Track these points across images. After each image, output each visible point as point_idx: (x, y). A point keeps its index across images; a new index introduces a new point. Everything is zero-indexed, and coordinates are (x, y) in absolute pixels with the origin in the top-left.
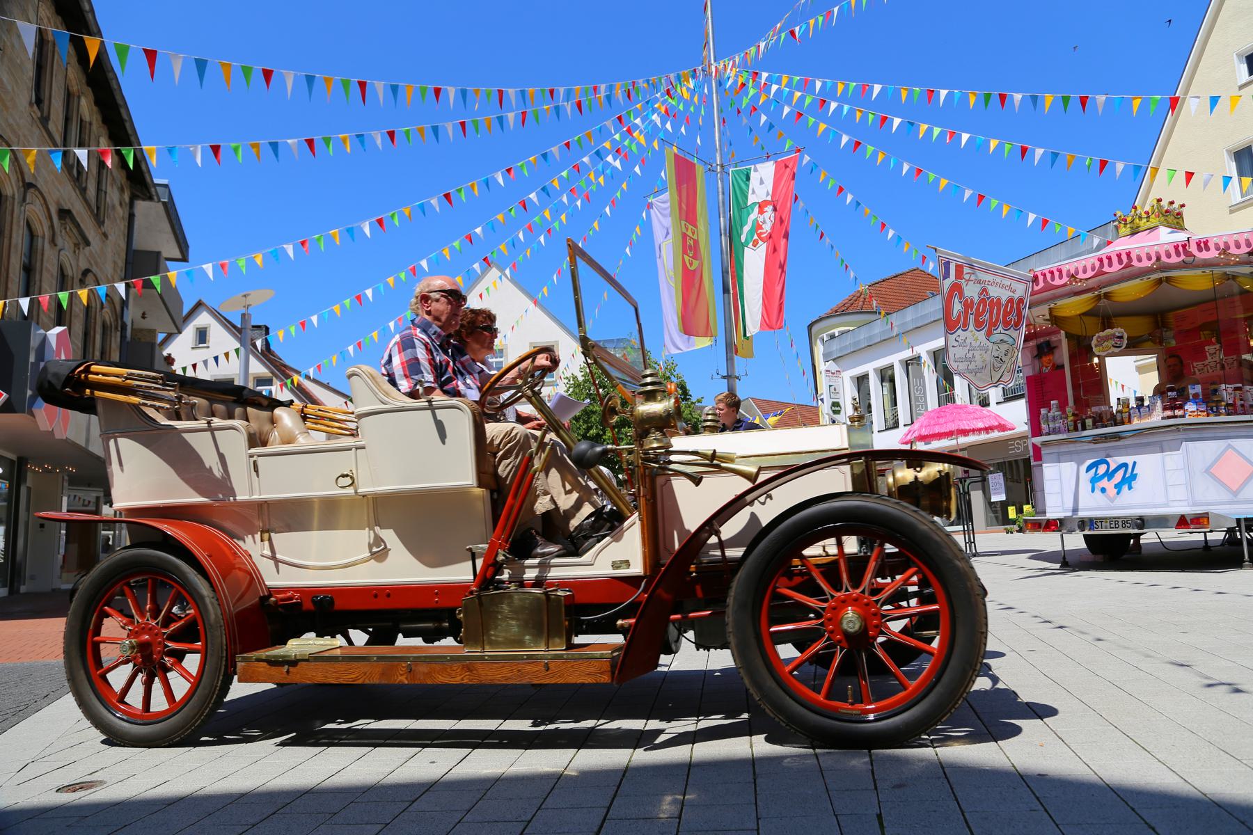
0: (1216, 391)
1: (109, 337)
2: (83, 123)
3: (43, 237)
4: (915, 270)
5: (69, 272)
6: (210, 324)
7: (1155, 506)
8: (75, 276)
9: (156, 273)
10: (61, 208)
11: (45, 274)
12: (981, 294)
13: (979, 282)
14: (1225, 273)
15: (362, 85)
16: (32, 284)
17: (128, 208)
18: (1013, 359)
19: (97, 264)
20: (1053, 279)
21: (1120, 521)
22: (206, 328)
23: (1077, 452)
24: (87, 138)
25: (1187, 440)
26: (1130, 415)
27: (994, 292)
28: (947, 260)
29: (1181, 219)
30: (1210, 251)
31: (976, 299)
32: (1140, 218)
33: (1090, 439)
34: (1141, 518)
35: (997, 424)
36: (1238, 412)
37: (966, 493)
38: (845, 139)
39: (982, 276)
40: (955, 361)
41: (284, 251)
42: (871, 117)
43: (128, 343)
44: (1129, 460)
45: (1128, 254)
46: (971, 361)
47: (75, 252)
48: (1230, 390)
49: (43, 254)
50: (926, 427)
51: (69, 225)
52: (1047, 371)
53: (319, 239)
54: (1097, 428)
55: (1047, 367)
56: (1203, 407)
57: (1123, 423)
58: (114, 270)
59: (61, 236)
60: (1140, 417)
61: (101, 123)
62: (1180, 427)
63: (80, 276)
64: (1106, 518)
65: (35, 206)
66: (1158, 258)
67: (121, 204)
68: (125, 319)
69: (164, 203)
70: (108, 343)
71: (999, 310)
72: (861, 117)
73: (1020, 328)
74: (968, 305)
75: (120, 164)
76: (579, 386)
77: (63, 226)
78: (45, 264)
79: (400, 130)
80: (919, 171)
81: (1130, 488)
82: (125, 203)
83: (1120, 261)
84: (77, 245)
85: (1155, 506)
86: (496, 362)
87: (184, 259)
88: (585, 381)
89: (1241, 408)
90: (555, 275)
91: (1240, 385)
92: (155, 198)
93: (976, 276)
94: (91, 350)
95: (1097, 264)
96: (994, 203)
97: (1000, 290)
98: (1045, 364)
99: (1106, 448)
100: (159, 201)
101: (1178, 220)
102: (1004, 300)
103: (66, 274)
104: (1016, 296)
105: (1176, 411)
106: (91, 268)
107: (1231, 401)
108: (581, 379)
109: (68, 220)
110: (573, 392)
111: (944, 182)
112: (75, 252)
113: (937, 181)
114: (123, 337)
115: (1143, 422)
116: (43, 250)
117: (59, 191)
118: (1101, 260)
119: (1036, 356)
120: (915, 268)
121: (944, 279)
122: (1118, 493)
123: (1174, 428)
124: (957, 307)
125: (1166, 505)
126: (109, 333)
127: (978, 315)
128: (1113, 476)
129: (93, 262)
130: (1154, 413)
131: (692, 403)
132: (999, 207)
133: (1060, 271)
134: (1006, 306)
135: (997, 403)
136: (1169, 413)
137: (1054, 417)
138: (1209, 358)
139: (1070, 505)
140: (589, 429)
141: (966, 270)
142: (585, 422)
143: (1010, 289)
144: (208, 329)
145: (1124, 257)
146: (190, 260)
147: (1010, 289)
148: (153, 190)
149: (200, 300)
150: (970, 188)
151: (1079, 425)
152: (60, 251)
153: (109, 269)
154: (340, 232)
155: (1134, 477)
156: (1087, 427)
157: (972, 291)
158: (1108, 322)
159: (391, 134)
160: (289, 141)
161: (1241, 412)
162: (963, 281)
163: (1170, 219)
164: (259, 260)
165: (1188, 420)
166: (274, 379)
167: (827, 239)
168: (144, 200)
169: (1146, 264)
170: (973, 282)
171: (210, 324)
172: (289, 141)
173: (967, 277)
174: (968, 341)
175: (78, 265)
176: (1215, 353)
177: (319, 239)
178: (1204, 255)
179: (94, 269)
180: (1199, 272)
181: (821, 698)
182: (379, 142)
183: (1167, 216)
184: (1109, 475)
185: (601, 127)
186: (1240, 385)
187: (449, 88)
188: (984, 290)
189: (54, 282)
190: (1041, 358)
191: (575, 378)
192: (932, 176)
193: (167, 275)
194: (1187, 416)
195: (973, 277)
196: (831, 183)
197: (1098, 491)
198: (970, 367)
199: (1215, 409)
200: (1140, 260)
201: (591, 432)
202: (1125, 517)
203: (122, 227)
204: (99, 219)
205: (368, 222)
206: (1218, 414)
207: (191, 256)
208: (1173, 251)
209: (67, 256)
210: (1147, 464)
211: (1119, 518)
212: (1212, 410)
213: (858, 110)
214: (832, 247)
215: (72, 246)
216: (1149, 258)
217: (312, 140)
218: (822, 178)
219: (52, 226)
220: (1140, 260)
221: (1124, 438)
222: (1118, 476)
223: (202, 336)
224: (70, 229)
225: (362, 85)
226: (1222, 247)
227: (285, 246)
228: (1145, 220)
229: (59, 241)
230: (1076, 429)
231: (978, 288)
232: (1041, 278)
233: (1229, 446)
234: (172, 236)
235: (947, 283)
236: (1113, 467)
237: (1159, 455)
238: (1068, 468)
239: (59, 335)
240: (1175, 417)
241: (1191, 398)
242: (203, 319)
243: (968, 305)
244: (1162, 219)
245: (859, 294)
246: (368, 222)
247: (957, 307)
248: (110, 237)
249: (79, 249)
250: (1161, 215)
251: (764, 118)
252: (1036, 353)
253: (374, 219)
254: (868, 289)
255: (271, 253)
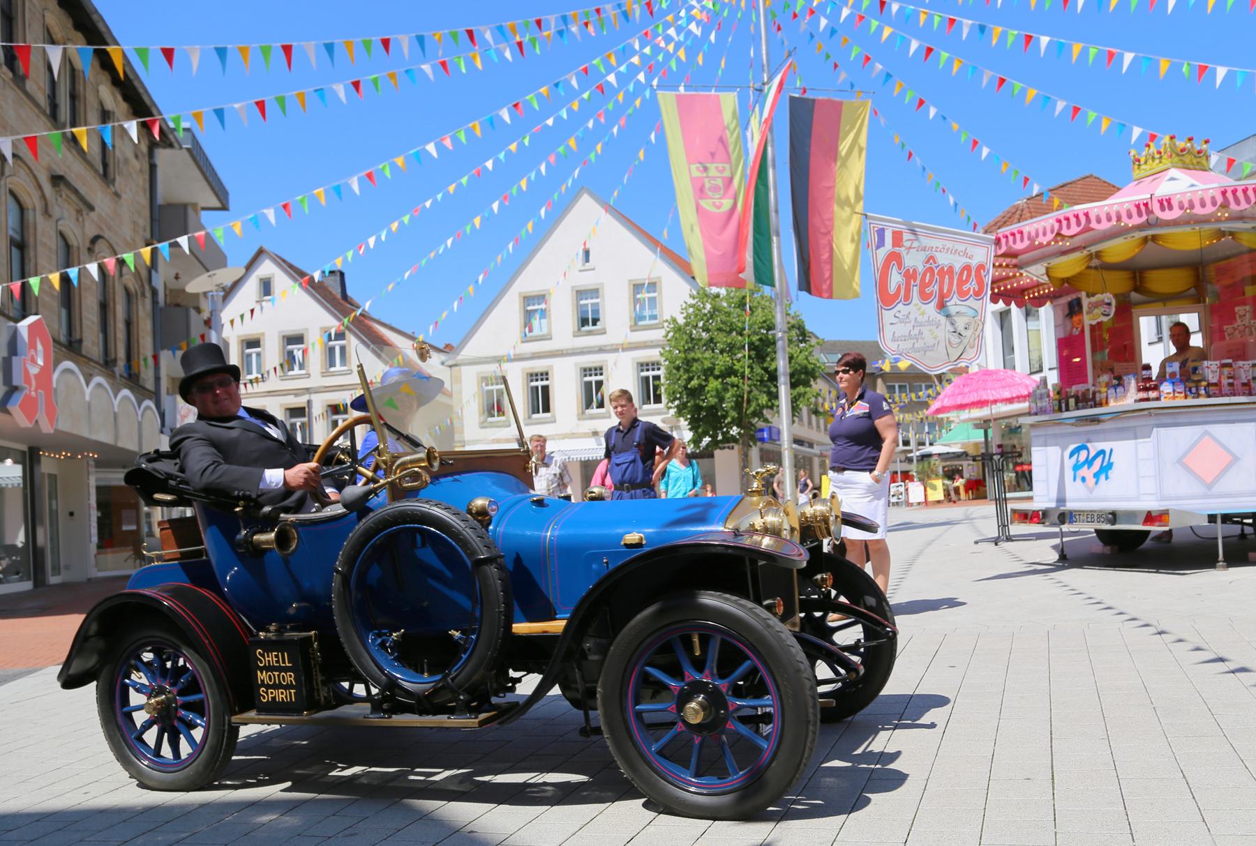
0: (1195, 369)
1: (135, 305)
2: (76, 73)
3: (34, 210)
4: (1087, 177)
5: (73, 241)
6: (273, 274)
7: (1128, 500)
8: (81, 245)
9: (184, 232)
10: (54, 174)
11: (40, 249)
12: (927, 262)
13: (924, 249)
14: (1220, 230)
15: (287, 49)
16: (27, 261)
17: (147, 158)
18: (977, 333)
19: (110, 228)
20: (1015, 242)
21: (1096, 514)
22: (270, 278)
23: (1063, 435)
24: (82, 89)
25: (1159, 426)
26: (1107, 398)
27: (943, 260)
28: (881, 227)
29: (1204, 158)
30: (1173, 212)
31: (921, 269)
32: (1153, 158)
33: (1073, 421)
34: (1114, 514)
35: (1026, 393)
36: (1223, 393)
37: (999, 470)
38: (914, 45)
39: (925, 241)
40: (894, 340)
41: (265, 217)
42: (937, 19)
43: (161, 309)
44: (1105, 446)
45: (1087, 215)
46: (918, 339)
47: (78, 219)
48: (1214, 368)
49: (35, 228)
50: (950, 396)
51: (65, 191)
52: (1077, 333)
53: (302, 201)
54: (1078, 409)
55: (1077, 328)
56: (1180, 388)
57: (1101, 405)
58: (135, 230)
59: (58, 205)
60: (1116, 399)
61: (98, 68)
62: (1152, 411)
63: (88, 244)
64: (1083, 511)
65: (18, 177)
66: (1119, 219)
67: (136, 156)
68: (154, 283)
69: (188, 150)
70: (135, 312)
71: (951, 279)
72: (926, 22)
73: (982, 298)
74: (909, 276)
75: (131, 111)
76: (679, 329)
77: (59, 193)
78: (39, 237)
79: (366, 79)
80: (1002, 81)
81: (1107, 478)
82: (142, 153)
83: (1078, 223)
84: (79, 212)
85: (1128, 500)
86: (592, 304)
87: (224, 208)
88: (687, 324)
89: (1228, 388)
90: (511, 244)
91: (1230, 361)
92: (176, 144)
93: (919, 242)
94: (112, 322)
95: (1057, 226)
96: (1092, 116)
97: (951, 256)
98: (1075, 324)
99: (1088, 433)
100: (181, 148)
101: (1199, 160)
102: (957, 268)
103: (70, 243)
104: (974, 263)
105: (1150, 393)
106: (102, 234)
107: (1215, 380)
108: (681, 321)
109: (62, 187)
110: (673, 337)
111: (1032, 93)
112: (78, 219)
113: (1023, 91)
114: (155, 302)
115: (1119, 404)
116: (35, 224)
117: (49, 155)
118: (1059, 221)
119: (1068, 315)
120: (1087, 174)
121: (878, 248)
122: (1096, 483)
123: (1146, 412)
124: (895, 279)
125: (1137, 499)
126: (135, 301)
127: (923, 286)
128: (1092, 464)
129: (104, 227)
130: (1129, 394)
131: (811, 346)
132: (1097, 122)
133: (1021, 233)
134: (961, 274)
135: (1149, 344)
136: (1143, 395)
137: (1041, 395)
138: (1239, 320)
139: (1054, 494)
140: (690, 379)
141: (907, 236)
142: (687, 371)
143: (966, 254)
144: (272, 280)
145: (1083, 219)
146: (231, 208)
147: (966, 254)
148: (171, 137)
149: (261, 248)
150: (1064, 98)
151: (1063, 405)
152: (57, 221)
153: (127, 231)
154: (326, 191)
155: (1110, 465)
156: (1071, 408)
157: (914, 260)
158: (1140, 276)
159: (356, 85)
160: (236, 106)
161: (1228, 392)
162: (903, 249)
163: (1187, 159)
164: (238, 228)
165: (1164, 402)
166: (347, 333)
167: (917, 159)
168: (165, 147)
169: (1105, 226)
170: (915, 250)
171: (273, 274)
172: (236, 106)
173: (907, 244)
174: (912, 317)
175: (84, 234)
176: (1245, 315)
177: (302, 201)
178: (1167, 215)
179: (107, 234)
180: (1188, 229)
181: (599, 712)
182: (342, 95)
183: (1183, 155)
184: (1089, 462)
185: (624, 48)
186: (1230, 361)
187: (400, 37)
188: (931, 258)
189: (54, 257)
190: (1072, 317)
191: (674, 320)
192: (1018, 86)
193: (140, 252)
194: (1162, 398)
195: (915, 244)
196: (909, 95)
197: (1079, 480)
198: (916, 346)
199: (1194, 390)
200: (1099, 221)
201: (693, 383)
202: (1100, 511)
203: (141, 182)
204: (106, 175)
205: (356, 178)
206: (1198, 395)
207: (232, 204)
208: (1134, 211)
209: (70, 227)
210: (1123, 450)
211: (1095, 511)
212: (1190, 390)
213: (924, 12)
214: (924, 169)
215: (73, 213)
216: (1109, 219)
217: (263, 102)
218: (897, 90)
219: (43, 196)
220: (1099, 221)
221: (1103, 421)
222: (1097, 464)
223: (266, 287)
224: (67, 195)
225: (287, 49)
226: (1186, 205)
227: (265, 211)
228: (1157, 161)
229: (56, 211)
230: (1060, 410)
231: (922, 256)
232: (1003, 241)
233: (1206, 433)
234: (204, 183)
235: (882, 253)
236: (1092, 454)
237: (1133, 441)
238: (1053, 452)
239: (30, 327)
240: (1147, 400)
241: (1168, 377)
242: (267, 268)
243: (909, 276)
244: (1176, 159)
245: (1014, 210)
246: (356, 178)
247: (895, 279)
248: (124, 196)
249: (82, 215)
250: (1174, 155)
251: (823, 22)
252: (1067, 312)
253: (363, 173)
254: (1026, 203)
255: (251, 219)
